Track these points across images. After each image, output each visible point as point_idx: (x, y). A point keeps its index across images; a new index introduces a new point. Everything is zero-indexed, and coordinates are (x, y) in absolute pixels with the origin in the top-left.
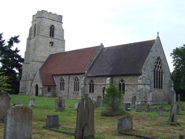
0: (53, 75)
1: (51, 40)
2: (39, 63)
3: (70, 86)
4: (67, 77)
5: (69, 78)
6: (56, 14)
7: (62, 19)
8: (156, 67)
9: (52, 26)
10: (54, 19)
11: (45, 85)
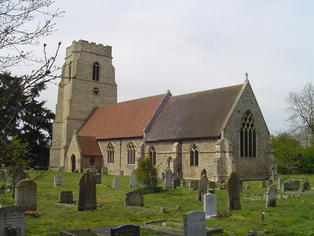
0: (97, 140)
2: (77, 121)
3: (122, 155)
4: (118, 143)
5: (121, 144)
6: (102, 45)
8: (244, 125)
9: (97, 63)
10: (99, 53)
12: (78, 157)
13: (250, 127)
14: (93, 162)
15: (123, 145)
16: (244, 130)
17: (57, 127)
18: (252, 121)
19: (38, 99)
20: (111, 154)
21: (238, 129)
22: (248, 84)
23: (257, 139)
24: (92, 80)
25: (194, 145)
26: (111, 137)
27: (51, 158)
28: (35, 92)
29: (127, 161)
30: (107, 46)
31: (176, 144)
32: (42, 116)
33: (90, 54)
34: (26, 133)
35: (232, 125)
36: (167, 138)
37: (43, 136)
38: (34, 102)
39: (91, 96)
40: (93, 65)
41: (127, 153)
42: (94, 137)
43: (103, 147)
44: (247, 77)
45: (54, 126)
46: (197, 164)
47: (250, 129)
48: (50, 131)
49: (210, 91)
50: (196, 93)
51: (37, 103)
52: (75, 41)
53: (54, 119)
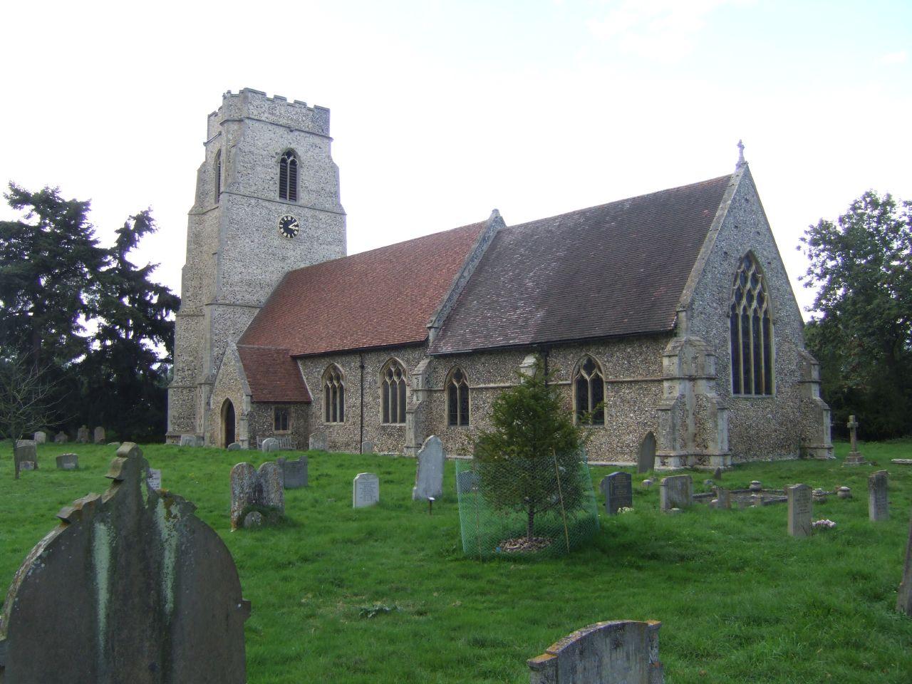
0: (295, 358)
1: (285, 210)
2: (239, 310)
3: (368, 399)
4: (355, 362)
7: (327, 122)
8: (739, 296)
9: (290, 153)
10: (292, 124)
11: (257, 402)
12: (242, 406)
13: (755, 304)
14: (285, 419)
15: (369, 369)
16: (740, 311)
17: (186, 330)
18: (759, 286)
19: (137, 258)
20: (335, 394)
21: (726, 309)
22: (747, 175)
23: (774, 340)
24: (278, 199)
25: (590, 361)
26: (335, 348)
27: (172, 413)
28: (127, 238)
29: (381, 416)
30: (316, 107)
31: (530, 360)
32: (148, 304)
33: (270, 127)
34: (104, 347)
35: (707, 295)
36: (502, 343)
37: (151, 357)
38: (125, 265)
39: (276, 240)
40: (279, 158)
41: (380, 392)
42: (287, 350)
43: (313, 380)
44: (741, 153)
45: (179, 332)
46: (465, 421)
47: (755, 310)
48: (170, 346)
49: (622, 203)
50: (582, 213)
51: (133, 269)
52: (229, 92)
53: (176, 309)
